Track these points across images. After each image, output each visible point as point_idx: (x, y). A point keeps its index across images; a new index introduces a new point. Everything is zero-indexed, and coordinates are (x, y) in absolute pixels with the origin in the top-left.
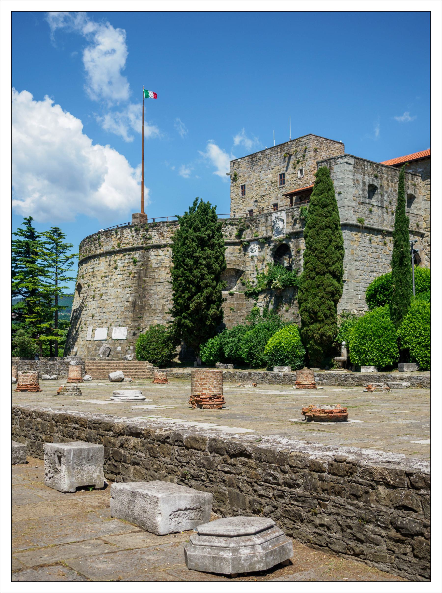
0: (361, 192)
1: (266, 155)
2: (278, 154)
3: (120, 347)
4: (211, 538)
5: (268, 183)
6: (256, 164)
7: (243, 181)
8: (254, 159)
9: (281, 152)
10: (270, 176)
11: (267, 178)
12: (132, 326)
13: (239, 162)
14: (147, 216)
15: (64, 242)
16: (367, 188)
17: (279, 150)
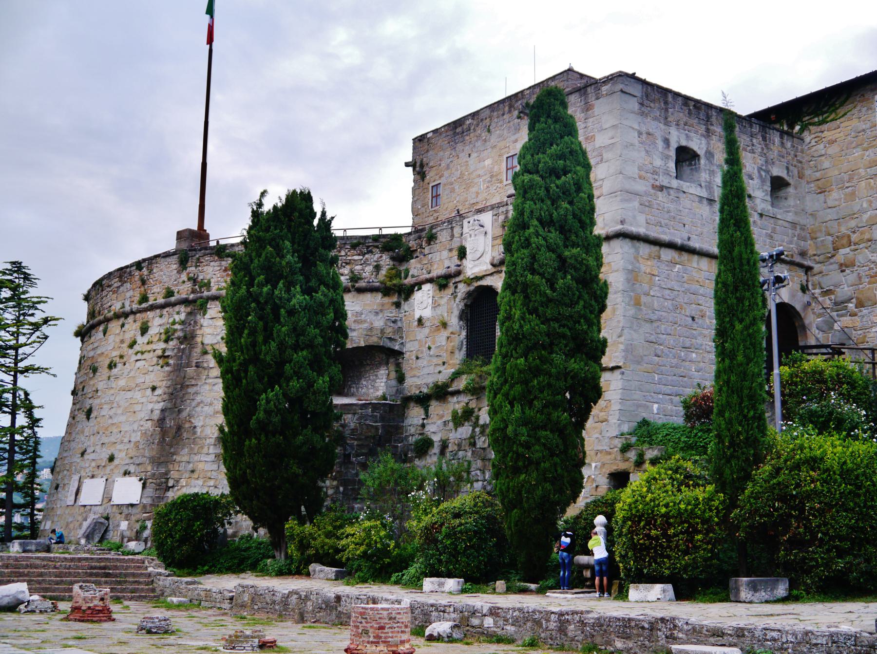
0: (658, 162)
1: (482, 120)
2: (505, 117)
3: (127, 522)
4: (785, 612)
5: (484, 178)
6: (461, 139)
7: (437, 177)
8: (459, 130)
9: (510, 112)
10: (488, 162)
11: (484, 167)
12: (154, 474)
13: (429, 139)
14: (208, 235)
15: (33, 293)
16: (673, 153)
17: (507, 108)
